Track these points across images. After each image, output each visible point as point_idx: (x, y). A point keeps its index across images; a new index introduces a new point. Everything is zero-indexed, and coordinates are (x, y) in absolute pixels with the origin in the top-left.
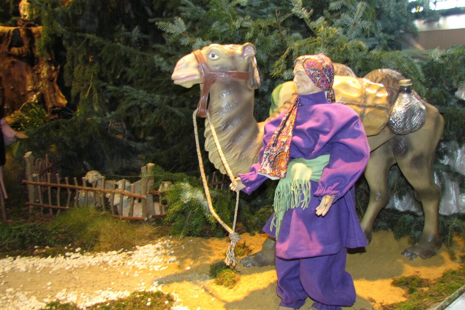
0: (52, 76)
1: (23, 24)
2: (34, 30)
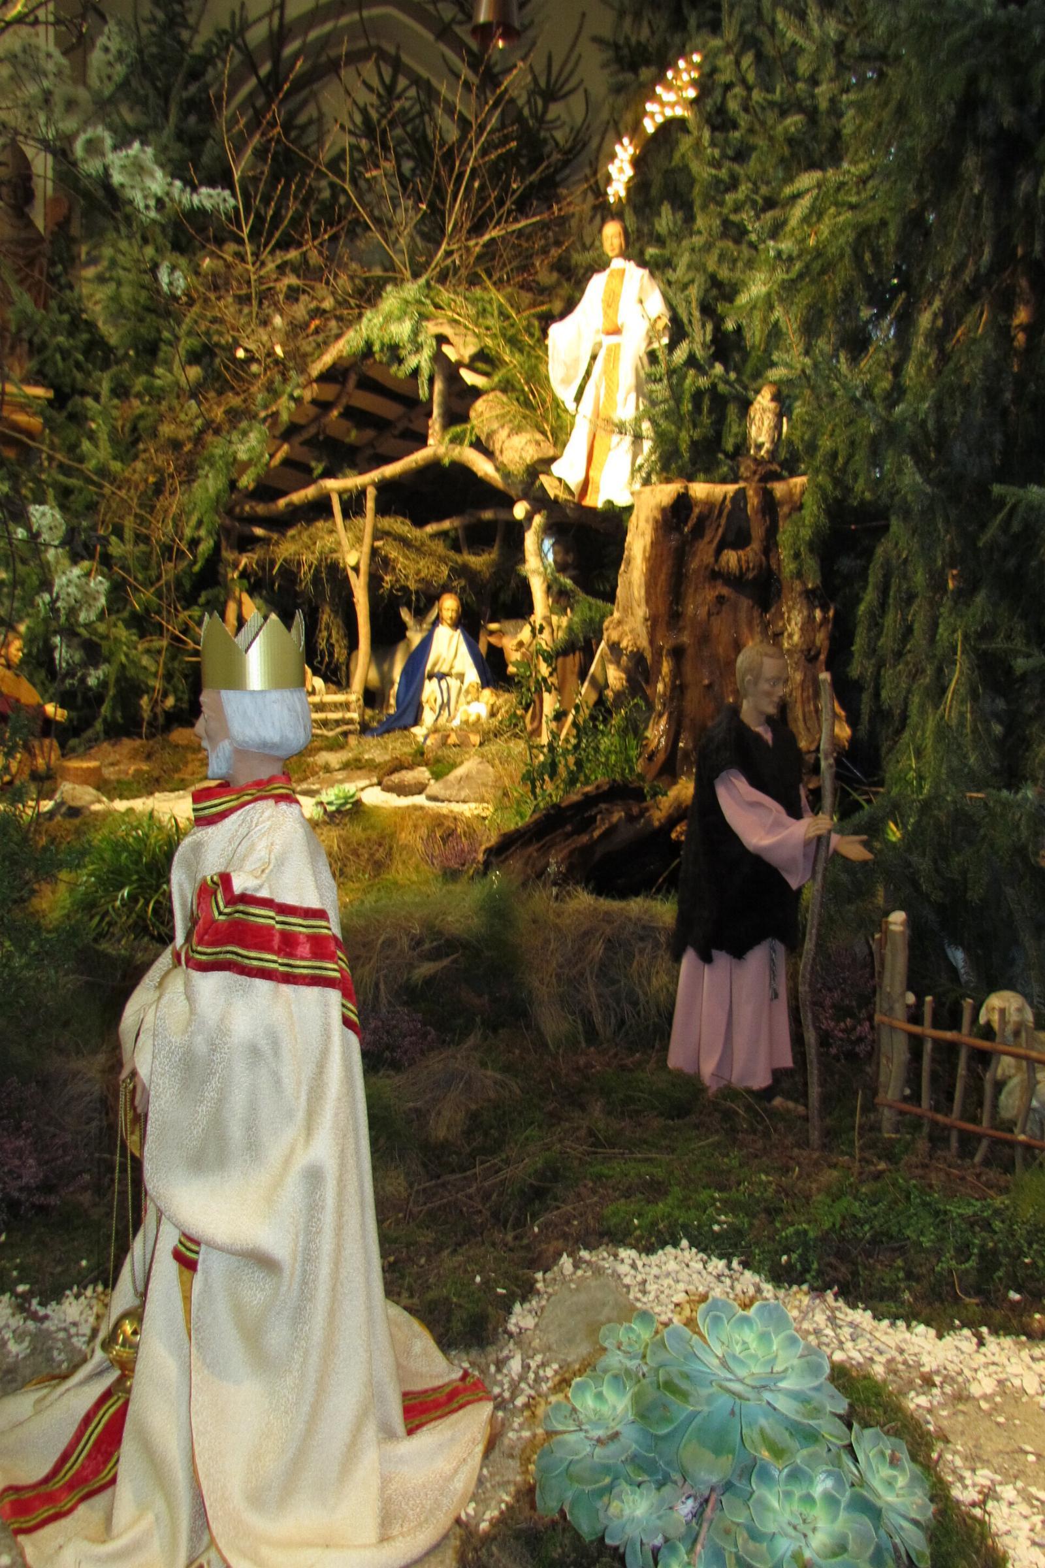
0: (813, 642)
1: (755, 473)
2: (779, 489)
